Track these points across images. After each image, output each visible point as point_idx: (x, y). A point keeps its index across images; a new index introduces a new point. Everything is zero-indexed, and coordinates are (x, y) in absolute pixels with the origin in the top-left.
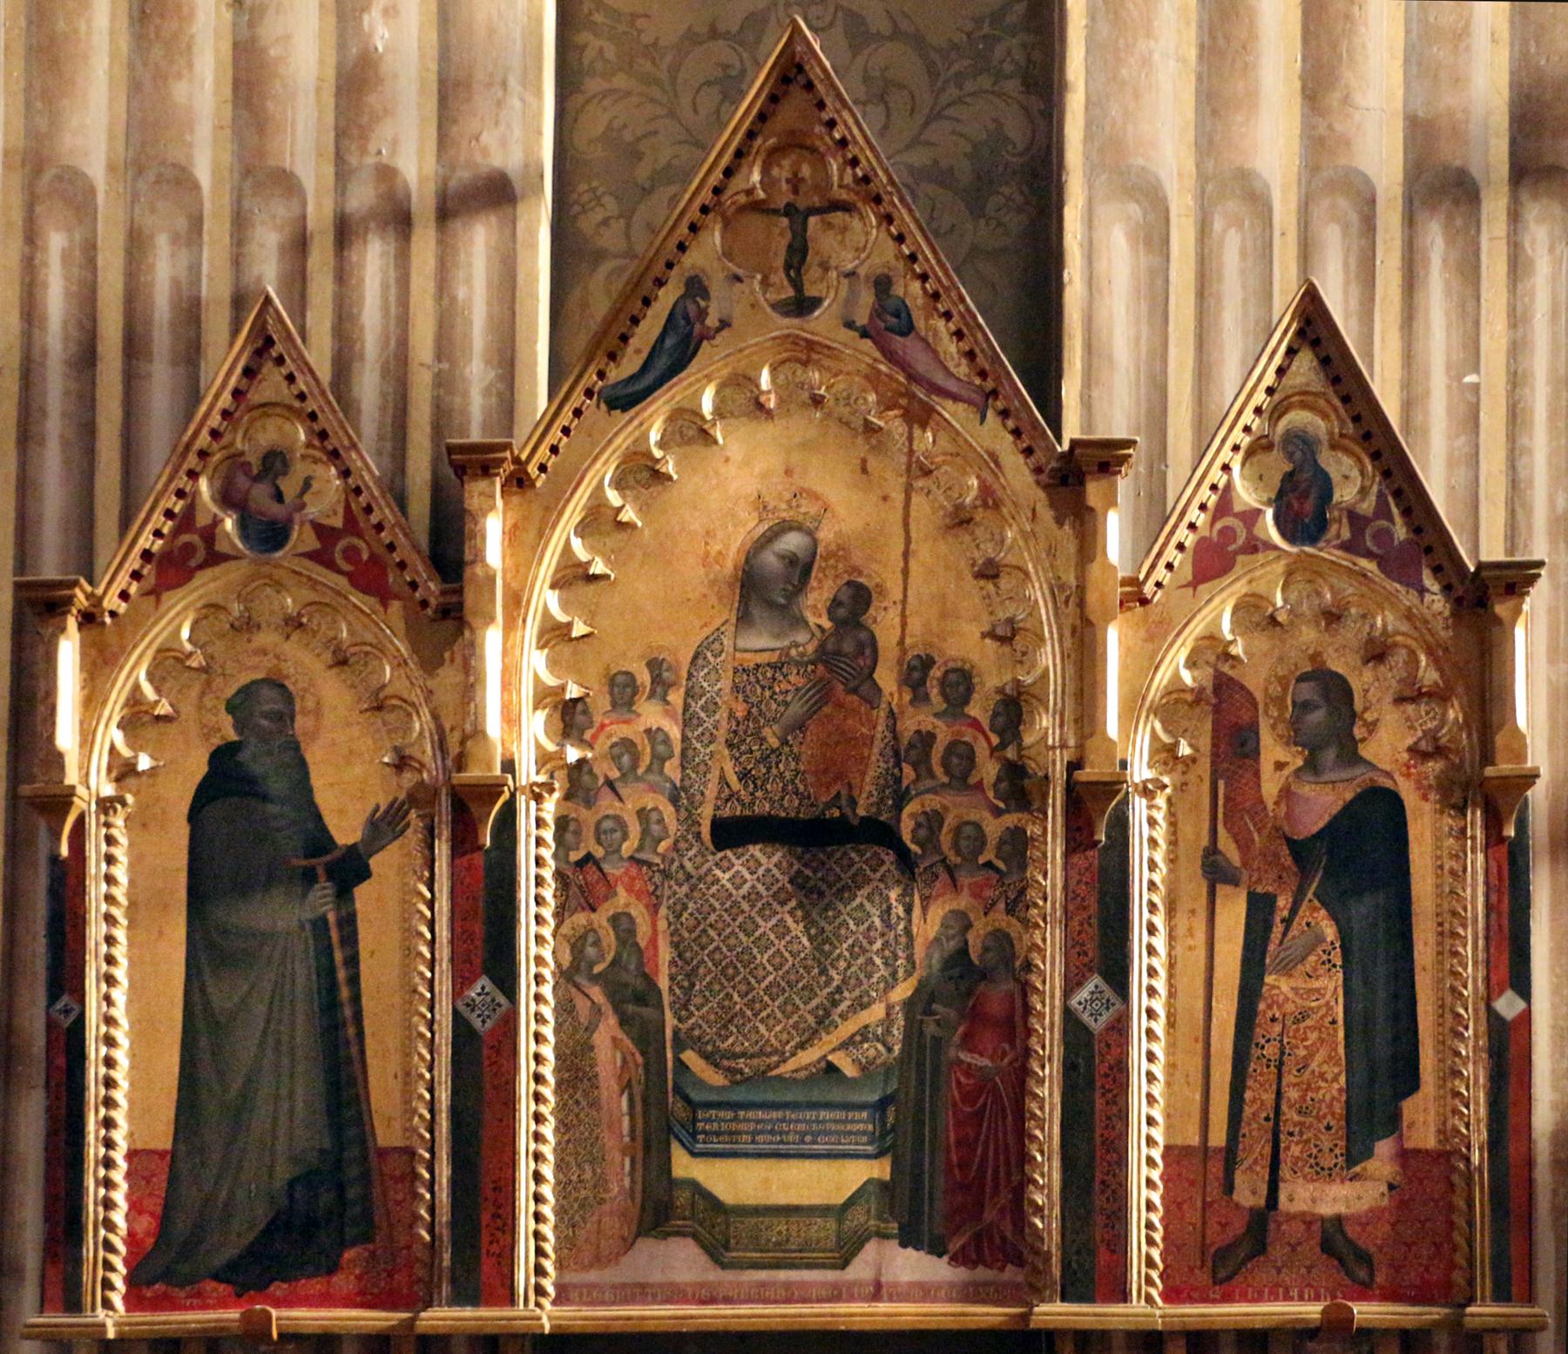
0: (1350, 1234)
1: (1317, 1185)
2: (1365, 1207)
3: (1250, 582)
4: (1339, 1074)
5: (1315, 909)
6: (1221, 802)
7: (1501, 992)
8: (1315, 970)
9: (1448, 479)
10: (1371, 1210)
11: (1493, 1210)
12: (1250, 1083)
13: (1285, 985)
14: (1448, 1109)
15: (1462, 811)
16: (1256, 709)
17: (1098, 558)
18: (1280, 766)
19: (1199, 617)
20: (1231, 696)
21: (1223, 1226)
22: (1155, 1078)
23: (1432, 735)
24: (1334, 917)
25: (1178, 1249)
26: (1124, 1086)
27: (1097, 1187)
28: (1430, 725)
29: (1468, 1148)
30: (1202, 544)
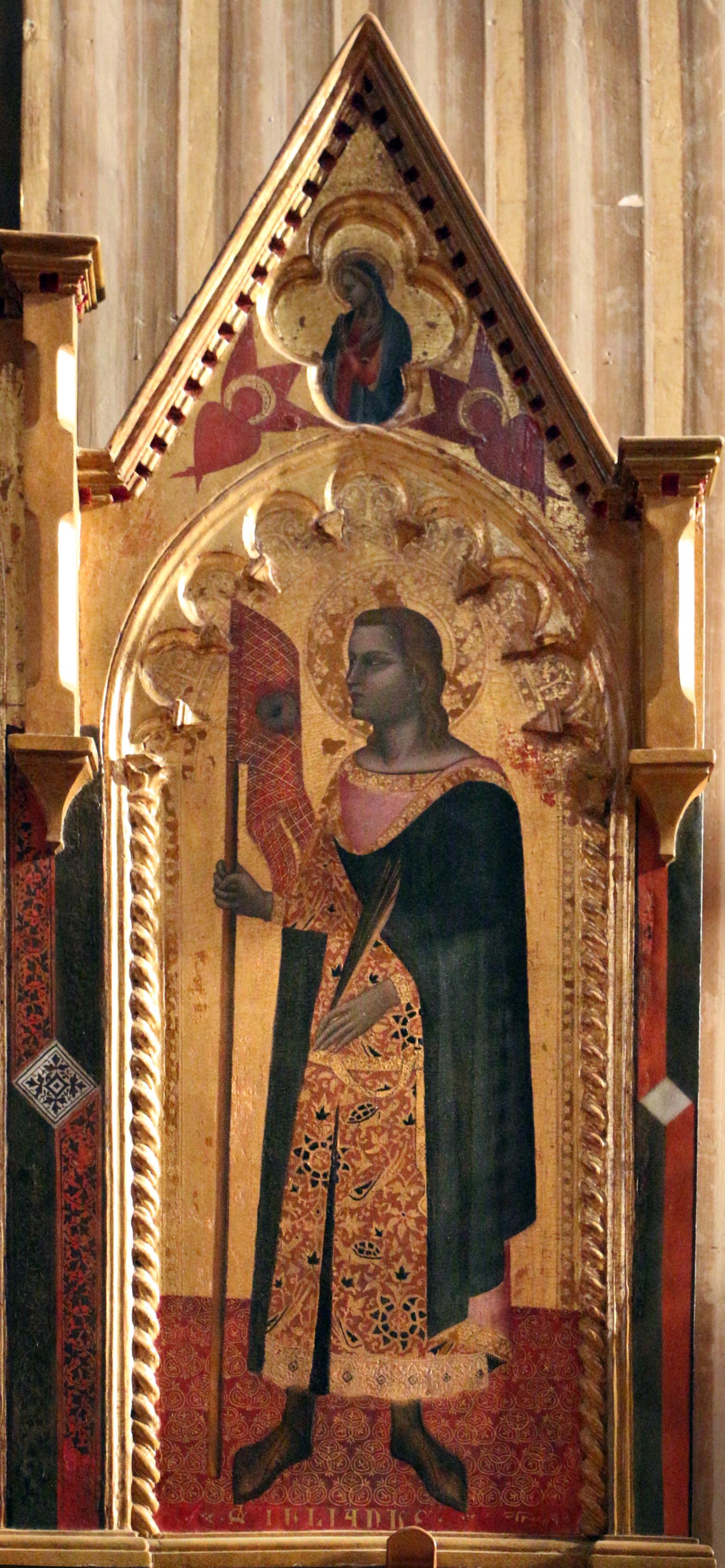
0: (432, 1431)
1: (386, 1358)
2: (457, 1390)
3: (283, 473)
4: (416, 1198)
5: (383, 957)
6: (242, 797)
7: (654, 1083)
8: (384, 1044)
9: (598, 352)
10: (464, 1395)
11: (637, 1397)
12: (288, 1207)
13: (339, 1066)
14: (577, 1250)
15: (601, 818)
16: (296, 662)
17: (43, 416)
18: (330, 746)
19: (205, 522)
20: (258, 643)
21: (250, 1416)
22: (147, 1197)
23: (561, 709)
24: (410, 966)
25: (184, 1448)
26: (100, 1208)
27: (59, 1354)
28: (558, 694)
29: (604, 1309)
30: (208, 412)
